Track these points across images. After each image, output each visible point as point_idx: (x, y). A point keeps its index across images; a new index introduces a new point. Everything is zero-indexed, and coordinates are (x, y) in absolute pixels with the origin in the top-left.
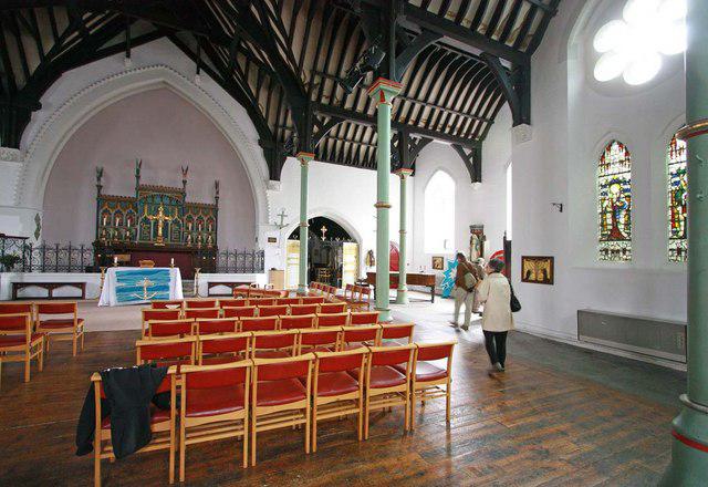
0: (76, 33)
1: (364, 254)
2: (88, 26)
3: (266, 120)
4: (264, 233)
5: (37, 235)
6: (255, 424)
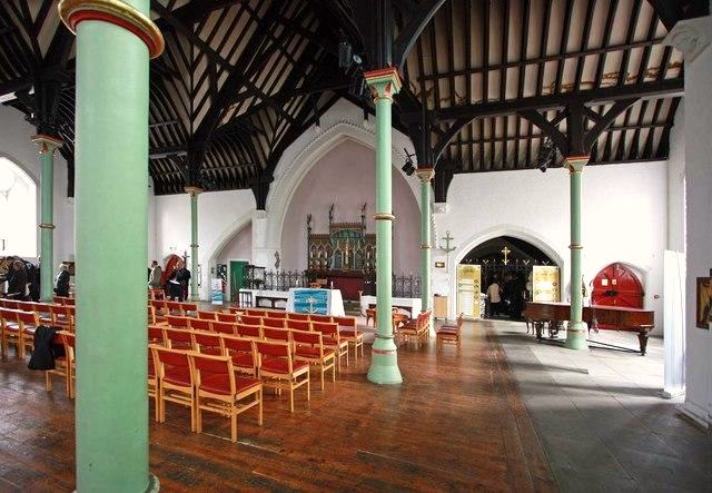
0: (294, 117)
2: (290, 113)
5: (277, 266)
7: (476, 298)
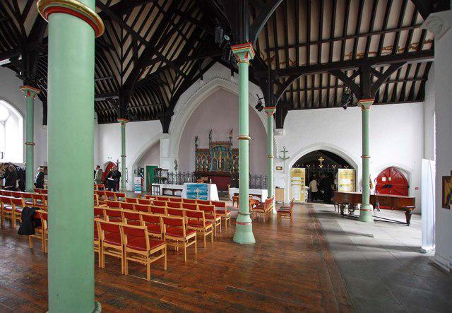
2: (184, 72)
5: (176, 169)
7: (302, 189)
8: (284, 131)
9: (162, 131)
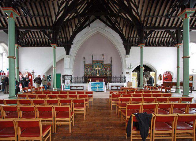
1: (158, 76)
3: (125, 36)
4: (125, 71)
6: (176, 135)
7: (136, 82)
8: (130, 56)
9: (65, 53)
